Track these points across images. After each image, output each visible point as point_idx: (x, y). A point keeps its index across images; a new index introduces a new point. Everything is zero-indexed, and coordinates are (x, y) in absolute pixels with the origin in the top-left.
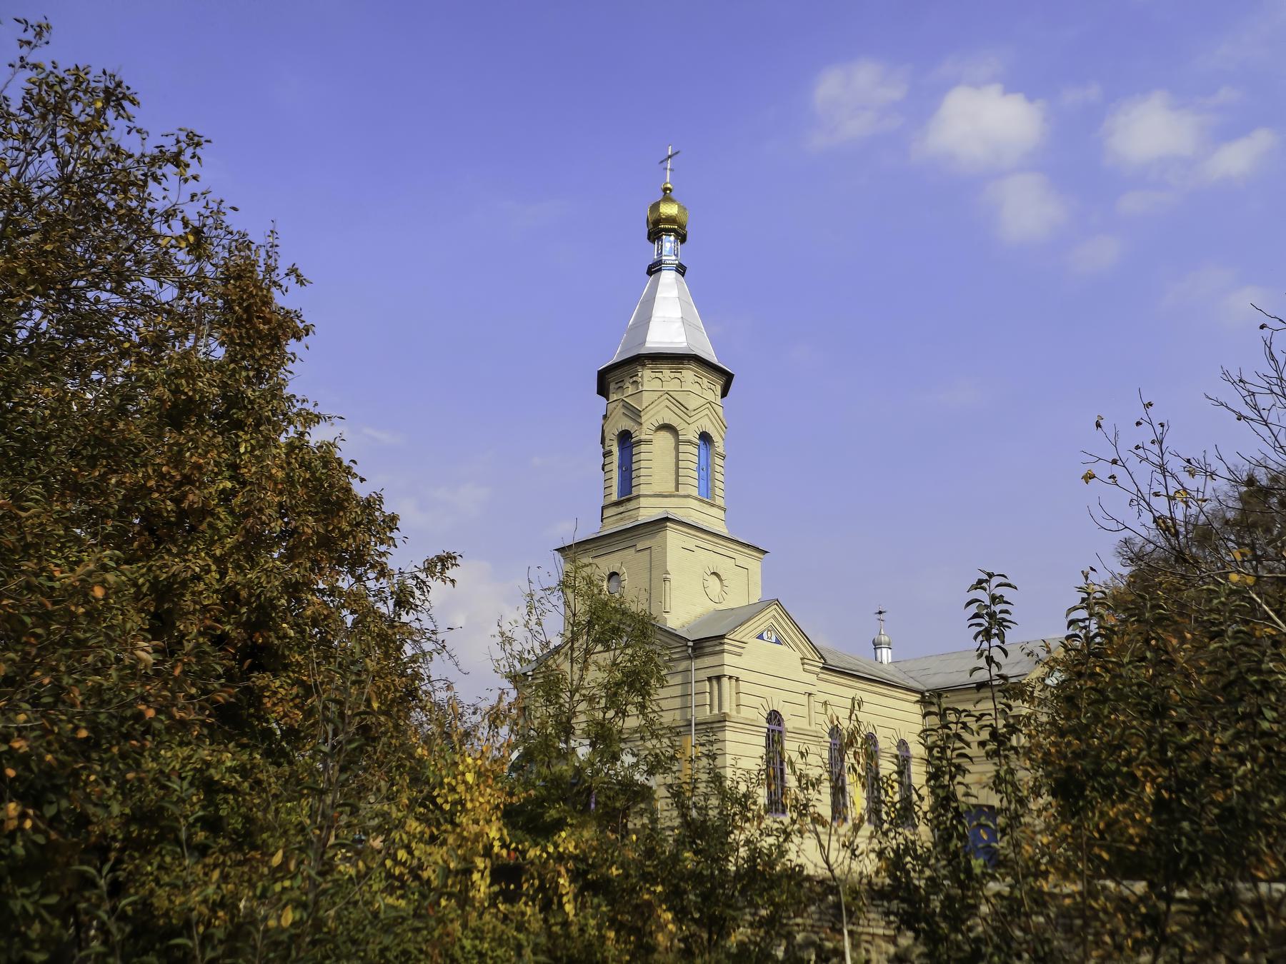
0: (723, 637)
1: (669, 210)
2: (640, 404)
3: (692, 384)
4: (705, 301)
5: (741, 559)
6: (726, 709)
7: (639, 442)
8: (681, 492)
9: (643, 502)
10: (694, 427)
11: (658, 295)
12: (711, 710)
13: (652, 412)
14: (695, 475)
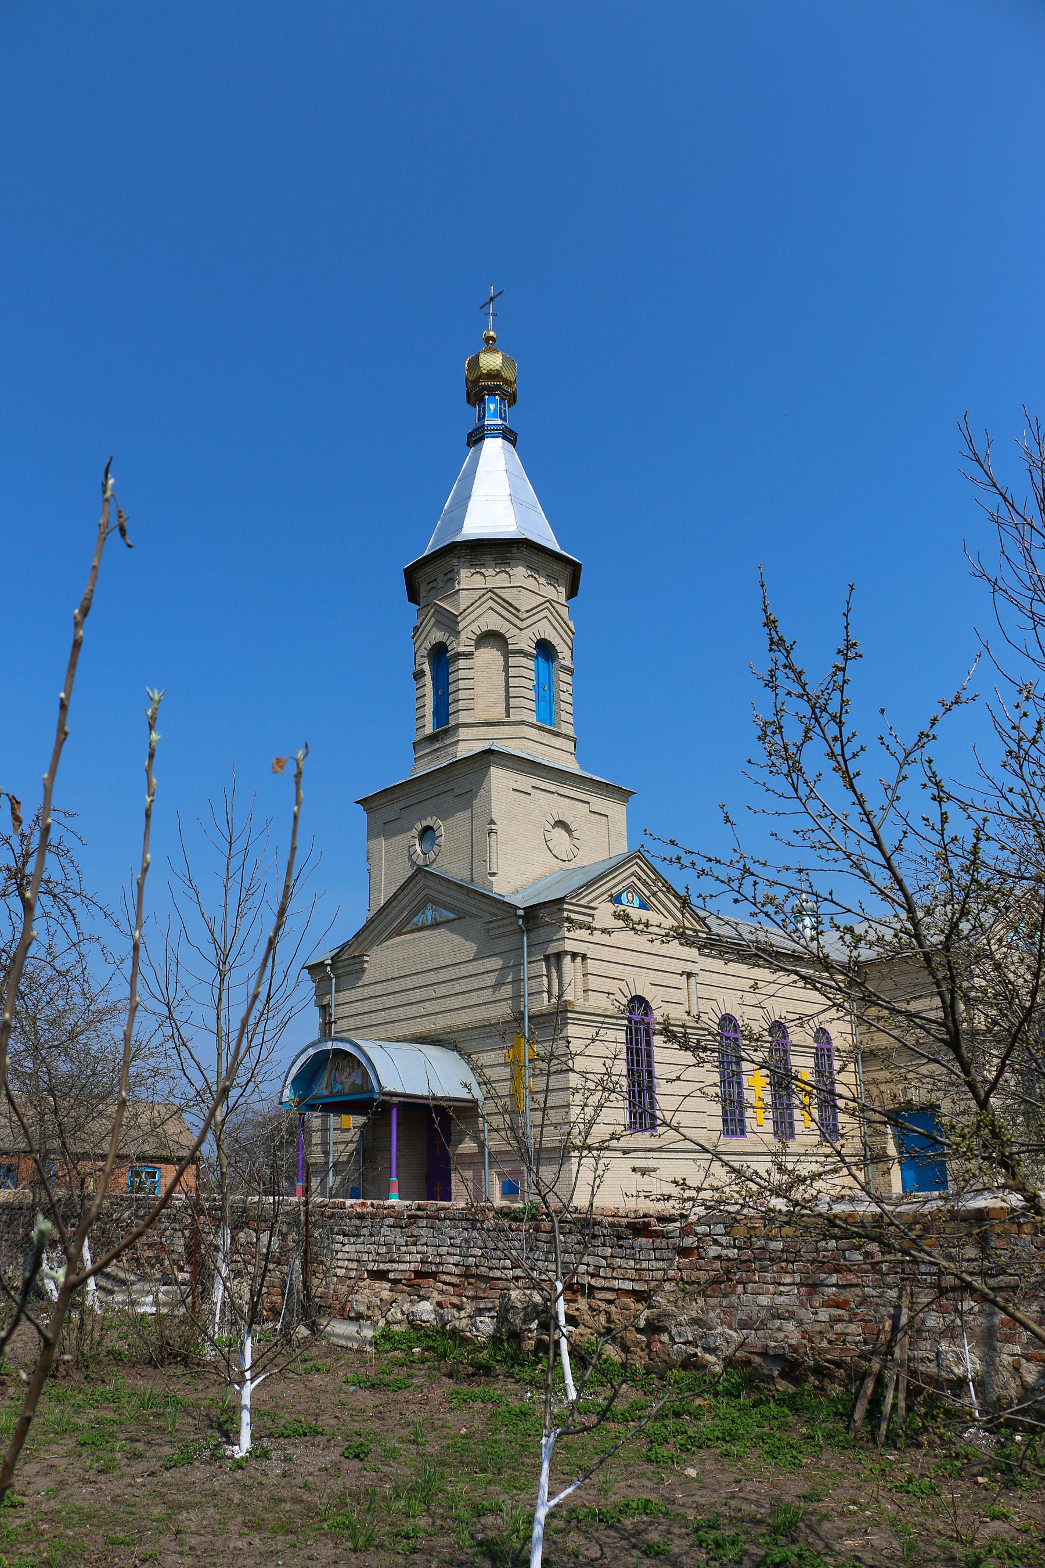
0: (561, 901)
1: (491, 361)
2: (457, 607)
3: (521, 582)
4: (542, 473)
5: (599, 803)
6: (568, 996)
7: (458, 656)
8: (512, 718)
9: (463, 733)
10: (528, 633)
11: (480, 469)
12: (549, 999)
13: (472, 617)
14: (532, 695)
